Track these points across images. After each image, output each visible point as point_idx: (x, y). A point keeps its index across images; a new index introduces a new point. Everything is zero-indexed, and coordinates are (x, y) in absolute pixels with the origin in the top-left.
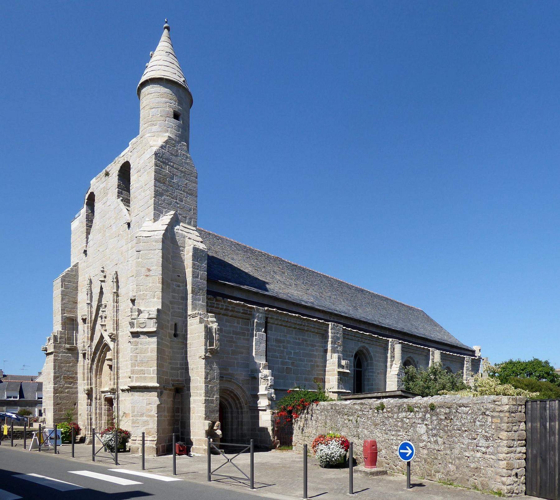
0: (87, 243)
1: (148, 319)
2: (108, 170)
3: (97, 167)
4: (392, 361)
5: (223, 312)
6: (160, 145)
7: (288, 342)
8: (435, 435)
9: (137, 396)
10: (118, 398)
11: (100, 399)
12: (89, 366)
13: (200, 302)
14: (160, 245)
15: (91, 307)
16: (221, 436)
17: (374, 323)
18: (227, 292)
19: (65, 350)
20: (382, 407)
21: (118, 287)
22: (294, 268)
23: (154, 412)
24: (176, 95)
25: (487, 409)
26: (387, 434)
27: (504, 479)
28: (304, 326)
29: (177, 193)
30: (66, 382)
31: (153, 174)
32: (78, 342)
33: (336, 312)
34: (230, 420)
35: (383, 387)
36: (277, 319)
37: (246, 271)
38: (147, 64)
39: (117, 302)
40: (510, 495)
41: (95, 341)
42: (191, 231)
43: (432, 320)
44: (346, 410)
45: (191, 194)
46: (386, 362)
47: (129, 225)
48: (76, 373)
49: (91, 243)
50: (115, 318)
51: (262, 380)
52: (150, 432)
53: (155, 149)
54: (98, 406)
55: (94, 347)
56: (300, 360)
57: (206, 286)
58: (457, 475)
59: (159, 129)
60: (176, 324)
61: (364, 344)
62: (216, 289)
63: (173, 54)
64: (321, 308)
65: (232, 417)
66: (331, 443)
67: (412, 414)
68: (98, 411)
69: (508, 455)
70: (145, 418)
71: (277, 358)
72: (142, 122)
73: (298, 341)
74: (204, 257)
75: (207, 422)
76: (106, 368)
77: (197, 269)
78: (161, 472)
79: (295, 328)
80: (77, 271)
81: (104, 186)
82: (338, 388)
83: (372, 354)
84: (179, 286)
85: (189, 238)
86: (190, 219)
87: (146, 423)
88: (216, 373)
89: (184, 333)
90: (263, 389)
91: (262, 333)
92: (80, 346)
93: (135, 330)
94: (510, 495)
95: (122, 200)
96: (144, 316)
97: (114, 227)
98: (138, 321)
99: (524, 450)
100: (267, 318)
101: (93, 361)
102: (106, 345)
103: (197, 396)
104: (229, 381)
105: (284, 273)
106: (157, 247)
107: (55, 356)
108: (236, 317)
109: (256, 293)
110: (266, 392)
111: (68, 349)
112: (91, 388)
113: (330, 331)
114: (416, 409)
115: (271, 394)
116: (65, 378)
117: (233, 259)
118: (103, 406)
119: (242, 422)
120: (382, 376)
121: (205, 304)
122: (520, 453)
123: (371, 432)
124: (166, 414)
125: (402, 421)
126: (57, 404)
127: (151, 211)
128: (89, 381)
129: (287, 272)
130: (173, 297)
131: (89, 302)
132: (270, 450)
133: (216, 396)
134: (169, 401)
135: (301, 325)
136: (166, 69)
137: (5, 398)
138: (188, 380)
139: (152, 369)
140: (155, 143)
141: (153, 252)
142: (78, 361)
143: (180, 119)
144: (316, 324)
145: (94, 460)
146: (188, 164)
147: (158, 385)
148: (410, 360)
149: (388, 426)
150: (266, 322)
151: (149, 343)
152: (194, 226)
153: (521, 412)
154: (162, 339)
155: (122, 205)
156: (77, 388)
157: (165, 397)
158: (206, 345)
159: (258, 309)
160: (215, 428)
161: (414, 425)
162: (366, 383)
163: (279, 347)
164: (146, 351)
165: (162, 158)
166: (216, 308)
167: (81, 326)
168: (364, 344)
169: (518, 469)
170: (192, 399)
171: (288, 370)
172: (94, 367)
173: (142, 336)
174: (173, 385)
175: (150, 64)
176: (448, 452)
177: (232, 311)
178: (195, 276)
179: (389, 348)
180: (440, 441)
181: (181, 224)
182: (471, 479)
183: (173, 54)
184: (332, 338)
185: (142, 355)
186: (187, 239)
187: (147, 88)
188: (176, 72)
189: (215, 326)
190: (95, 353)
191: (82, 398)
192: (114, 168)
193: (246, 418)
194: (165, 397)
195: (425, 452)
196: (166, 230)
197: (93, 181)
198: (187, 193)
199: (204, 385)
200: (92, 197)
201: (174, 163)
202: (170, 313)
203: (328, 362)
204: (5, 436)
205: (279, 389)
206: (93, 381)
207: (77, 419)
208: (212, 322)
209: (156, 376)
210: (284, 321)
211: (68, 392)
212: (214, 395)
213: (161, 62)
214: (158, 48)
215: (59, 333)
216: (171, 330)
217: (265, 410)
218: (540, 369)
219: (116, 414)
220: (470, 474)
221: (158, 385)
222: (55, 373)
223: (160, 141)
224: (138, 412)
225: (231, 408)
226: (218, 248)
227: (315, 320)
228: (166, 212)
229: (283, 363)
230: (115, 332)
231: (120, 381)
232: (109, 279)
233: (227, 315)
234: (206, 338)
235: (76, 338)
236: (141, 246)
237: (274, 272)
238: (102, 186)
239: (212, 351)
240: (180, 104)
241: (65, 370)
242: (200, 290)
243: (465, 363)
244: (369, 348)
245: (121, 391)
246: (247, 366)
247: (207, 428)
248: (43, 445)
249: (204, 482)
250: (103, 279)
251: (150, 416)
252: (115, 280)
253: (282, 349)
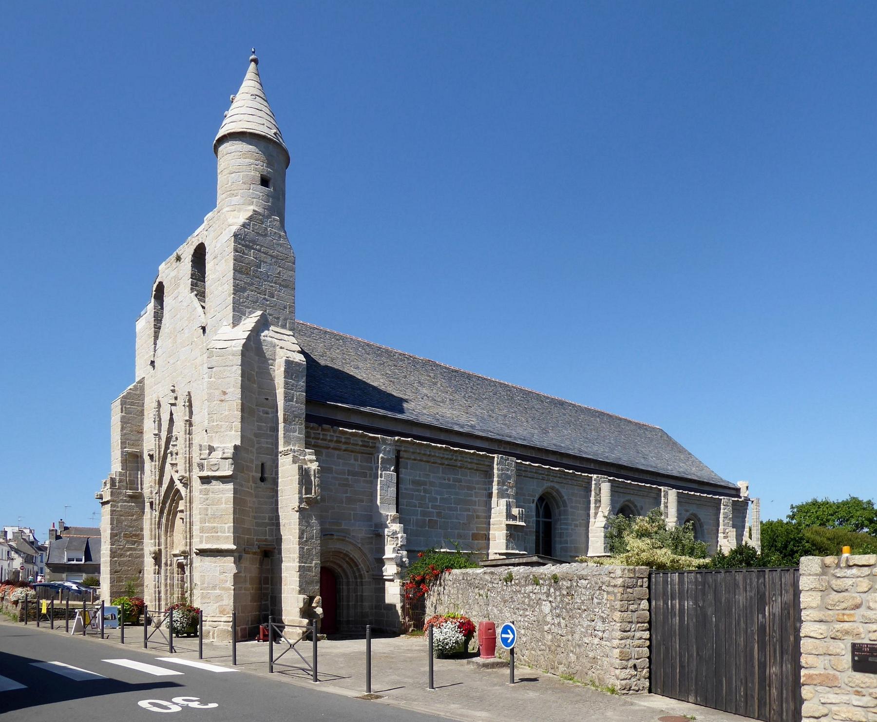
0: (155, 351)
2: (180, 253)
3: (167, 249)
4: (597, 508)
5: (332, 445)
6: (241, 223)
7: (432, 484)
8: (558, 616)
9: (208, 560)
10: (191, 564)
11: (171, 565)
13: (296, 434)
14: (238, 360)
15: (160, 438)
16: (321, 616)
17: (571, 452)
18: (340, 417)
19: (127, 496)
20: (509, 578)
22: (452, 375)
23: (230, 584)
25: (603, 583)
26: (515, 613)
27: (618, 672)
28: (456, 460)
29: (265, 285)
30: (128, 542)
32: (145, 486)
33: (508, 439)
34: (345, 594)
35: (583, 546)
36: (413, 453)
37: (375, 384)
38: (226, 112)
39: (189, 434)
40: (625, 692)
41: (165, 486)
42: (285, 337)
43: (675, 443)
44: (477, 582)
45: (286, 287)
46: (589, 508)
47: (204, 329)
48: (142, 529)
49: (159, 352)
51: (389, 539)
52: (224, 610)
53: (234, 229)
54: (168, 574)
55: (163, 494)
56: (450, 509)
57: (304, 411)
58: (577, 667)
60: (262, 464)
61: (552, 484)
62: (323, 413)
63: (262, 96)
64: (483, 434)
65: (348, 590)
66: (444, 624)
67: (538, 587)
68: (169, 581)
69: (623, 641)
70: (218, 591)
71: (415, 506)
72: (219, 192)
73: (447, 482)
74: (302, 372)
75: (302, 597)
76: (178, 522)
77: (292, 389)
78: (222, 661)
79: (442, 464)
80: (142, 389)
81: (175, 273)
82: (507, 548)
83: (565, 498)
84: (267, 413)
85: (281, 348)
86: (285, 319)
87: (219, 598)
88: (315, 530)
89: (274, 476)
90: (389, 552)
91: (391, 473)
92: (146, 492)
93: (205, 473)
94: (625, 692)
95: (196, 295)
96: (217, 455)
97: (186, 331)
99: (646, 635)
100: (398, 452)
101: (162, 512)
102: (178, 491)
104: (343, 540)
105: (435, 384)
108: (352, 452)
109: (384, 417)
110: (393, 555)
111: (130, 496)
112: (160, 550)
113: (495, 466)
114: (541, 582)
115: (402, 557)
116: (127, 534)
117: (357, 368)
118: (176, 575)
119: (362, 596)
120: (582, 530)
121: (302, 436)
122: (641, 638)
123: (501, 611)
124: (248, 585)
125: (529, 597)
127: (229, 312)
129: (441, 382)
130: (260, 428)
131: (157, 432)
132: (399, 635)
133: (316, 562)
134: (252, 567)
135: (451, 459)
136: (251, 118)
137: (65, 560)
138: (279, 540)
139: (226, 526)
140: (235, 220)
142: (143, 513)
143: (271, 184)
144: (475, 457)
145: (146, 647)
146: (281, 245)
147: (234, 547)
148: (631, 505)
149: (516, 603)
150: (398, 458)
151: (223, 491)
152: (290, 330)
153: (642, 586)
154: (242, 486)
155: (196, 300)
156: (142, 549)
157: (246, 564)
158: (300, 492)
159: (384, 441)
160: (314, 605)
161: (539, 602)
162: (557, 539)
163: (418, 491)
164: (219, 501)
165: (243, 241)
166: (322, 439)
167: (148, 465)
168: (552, 484)
169: (637, 659)
171: (432, 524)
172: (164, 521)
173: (214, 482)
174: (259, 547)
175: (229, 113)
176: (570, 637)
177: (346, 443)
178: (288, 398)
179: (593, 488)
180: (563, 622)
181: (272, 328)
182: (590, 672)
183: (262, 96)
184: (498, 476)
185: (214, 507)
186: (278, 349)
188: (264, 121)
189: (314, 466)
190: (164, 503)
191: (149, 562)
192: (187, 251)
193: (367, 591)
194: (246, 564)
195: (550, 637)
196: (248, 338)
197: (162, 267)
198: (280, 285)
199: (298, 547)
200: (161, 288)
201: (262, 246)
202: (254, 450)
203: (493, 511)
204: (44, 615)
205: (412, 548)
206: (163, 540)
207: (142, 592)
208: (311, 461)
210: (424, 454)
211: (130, 556)
212: (312, 560)
213: (246, 110)
214: (242, 89)
216: (256, 472)
217: (392, 580)
218: (858, 513)
220: (589, 665)
221: (234, 547)
222: (112, 529)
223: (242, 217)
224: (208, 583)
225: (347, 577)
226: (335, 353)
227: (472, 451)
228: (250, 313)
229: (424, 514)
230: (187, 475)
232: (180, 402)
233: (339, 450)
234: (301, 483)
235: (141, 481)
236: (214, 361)
237: (419, 382)
238: (173, 274)
239: (309, 501)
240: (269, 165)
242: (295, 417)
243: (722, 507)
244: (561, 490)
246: (369, 518)
247: (301, 605)
248: (89, 628)
249: (265, 673)
250: (173, 401)
251: (224, 589)
252: (187, 404)
253: (422, 494)
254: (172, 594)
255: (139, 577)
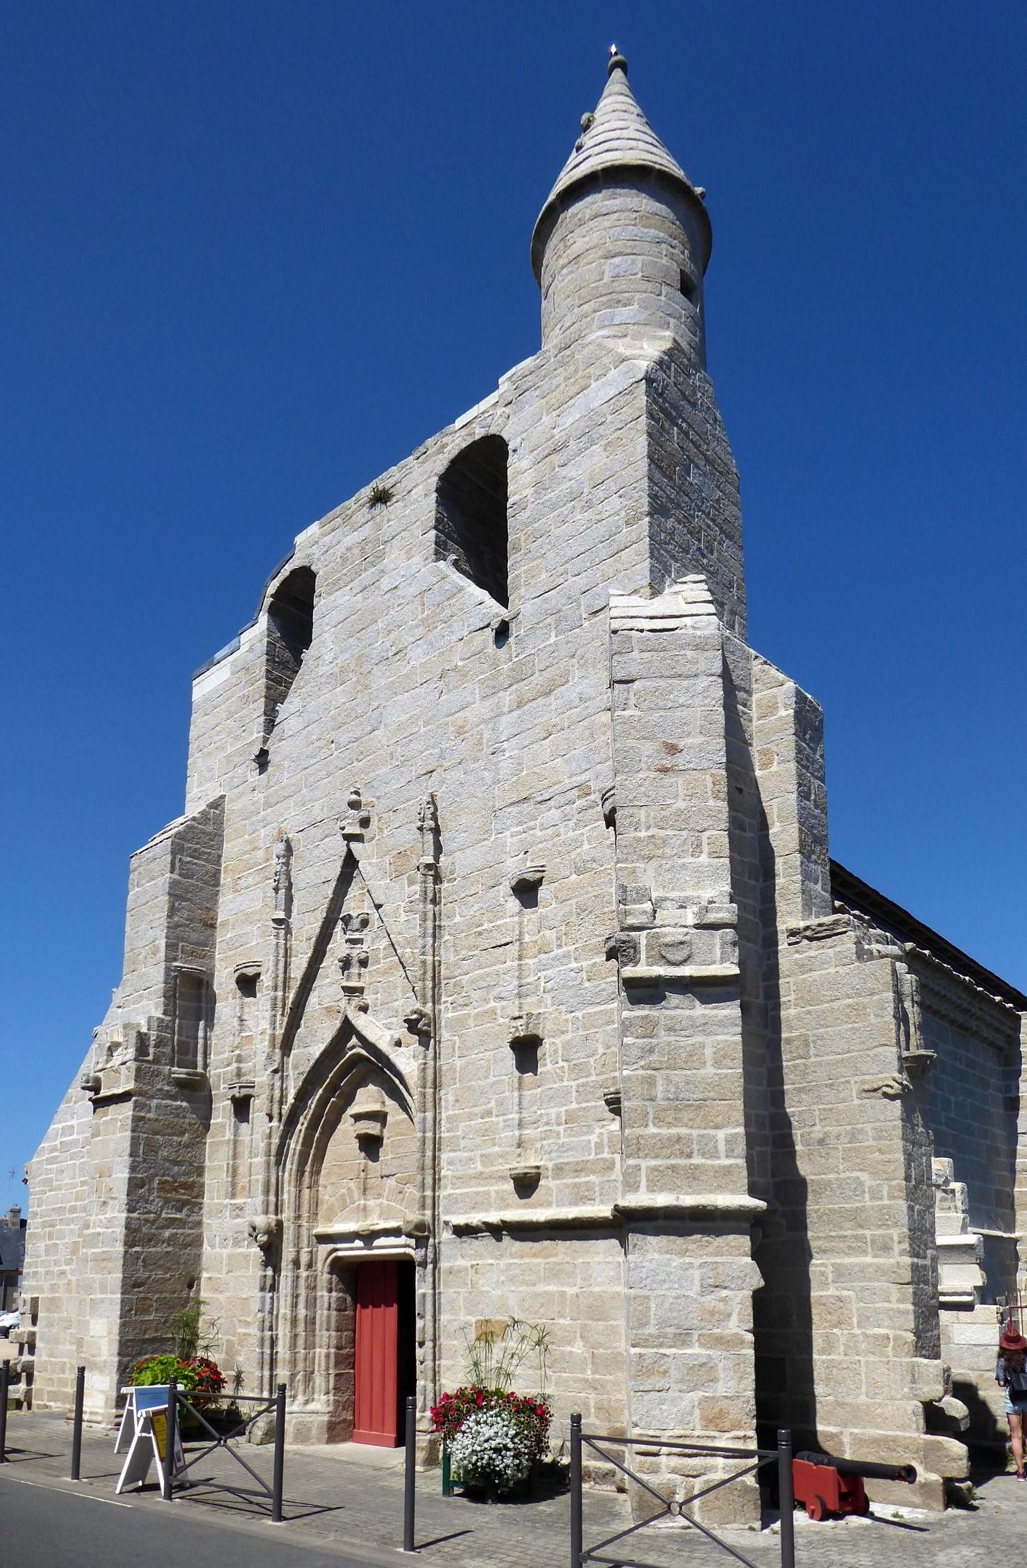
1: (698, 926)
10: (435, 1262)
11: (310, 1266)
12: (276, 1141)
21: (438, 849)
24: (685, 228)
31: (641, 445)
39: (435, 901)
50: (430, 958)
53: (643, 366)
54: (302, 1291)
59: (643, 316)
68: (302, 1312)
70: (696, 1350)
80: (219, 822)
87: (701, 1373)
93: (643, 969)
98: (657, 936)
103: (857, 1246)
106: (702, 666)
107: (137, 1106)
111: (180, 1084)
112: (279, 1224)
118: (322, 1294)
126: (137, 1285)
128: (272, 1198)
131: (281, 915)
139: (721, 1134)
141: (685, 683)
142: (207, 1127)
145: (76, 1475)
151: (705, 1027)
156: (199, 1224)
164: (694, 1057)
170: (818, 1265)
172: (295, 1144)
173: (674, 999)
185: (677, 1076)
187: (589, 199)
200: (302, 584)
209: (742, 1162)
215: (155, 1024)
217: (968, 1307)
219: (429, 1325)
222: (133, 1168)
223: (649, 349)
224: (663, 1323)
230: (428, 1009)
231: (442, 1193)
235: (206, 1046)
241: (166, 1159)
245: (446, 1235)
250: (357, 830)
251: (720, 1341)
254: (310, 1345)
255: (188, 1299)
